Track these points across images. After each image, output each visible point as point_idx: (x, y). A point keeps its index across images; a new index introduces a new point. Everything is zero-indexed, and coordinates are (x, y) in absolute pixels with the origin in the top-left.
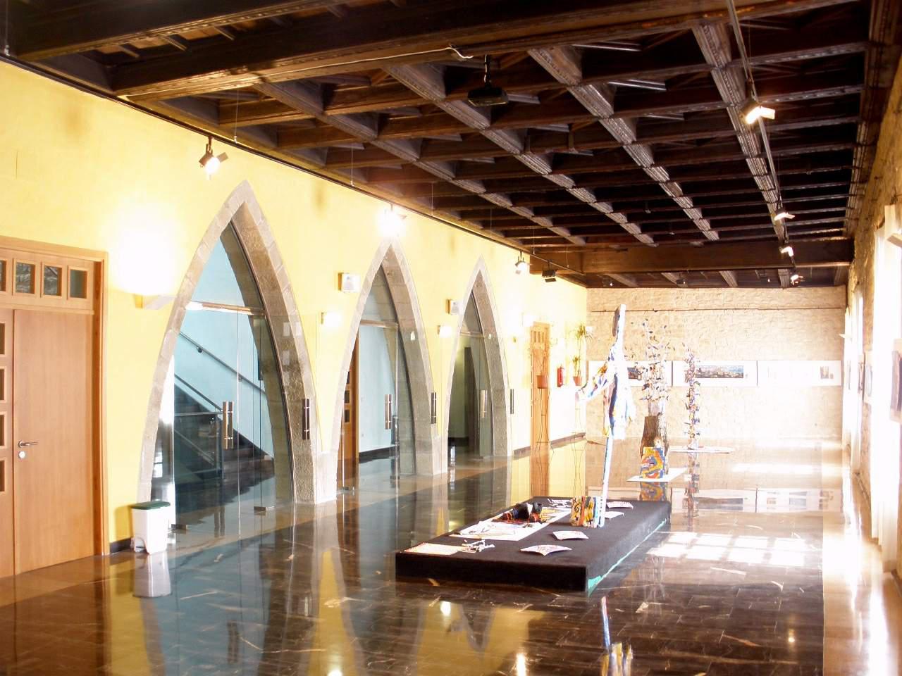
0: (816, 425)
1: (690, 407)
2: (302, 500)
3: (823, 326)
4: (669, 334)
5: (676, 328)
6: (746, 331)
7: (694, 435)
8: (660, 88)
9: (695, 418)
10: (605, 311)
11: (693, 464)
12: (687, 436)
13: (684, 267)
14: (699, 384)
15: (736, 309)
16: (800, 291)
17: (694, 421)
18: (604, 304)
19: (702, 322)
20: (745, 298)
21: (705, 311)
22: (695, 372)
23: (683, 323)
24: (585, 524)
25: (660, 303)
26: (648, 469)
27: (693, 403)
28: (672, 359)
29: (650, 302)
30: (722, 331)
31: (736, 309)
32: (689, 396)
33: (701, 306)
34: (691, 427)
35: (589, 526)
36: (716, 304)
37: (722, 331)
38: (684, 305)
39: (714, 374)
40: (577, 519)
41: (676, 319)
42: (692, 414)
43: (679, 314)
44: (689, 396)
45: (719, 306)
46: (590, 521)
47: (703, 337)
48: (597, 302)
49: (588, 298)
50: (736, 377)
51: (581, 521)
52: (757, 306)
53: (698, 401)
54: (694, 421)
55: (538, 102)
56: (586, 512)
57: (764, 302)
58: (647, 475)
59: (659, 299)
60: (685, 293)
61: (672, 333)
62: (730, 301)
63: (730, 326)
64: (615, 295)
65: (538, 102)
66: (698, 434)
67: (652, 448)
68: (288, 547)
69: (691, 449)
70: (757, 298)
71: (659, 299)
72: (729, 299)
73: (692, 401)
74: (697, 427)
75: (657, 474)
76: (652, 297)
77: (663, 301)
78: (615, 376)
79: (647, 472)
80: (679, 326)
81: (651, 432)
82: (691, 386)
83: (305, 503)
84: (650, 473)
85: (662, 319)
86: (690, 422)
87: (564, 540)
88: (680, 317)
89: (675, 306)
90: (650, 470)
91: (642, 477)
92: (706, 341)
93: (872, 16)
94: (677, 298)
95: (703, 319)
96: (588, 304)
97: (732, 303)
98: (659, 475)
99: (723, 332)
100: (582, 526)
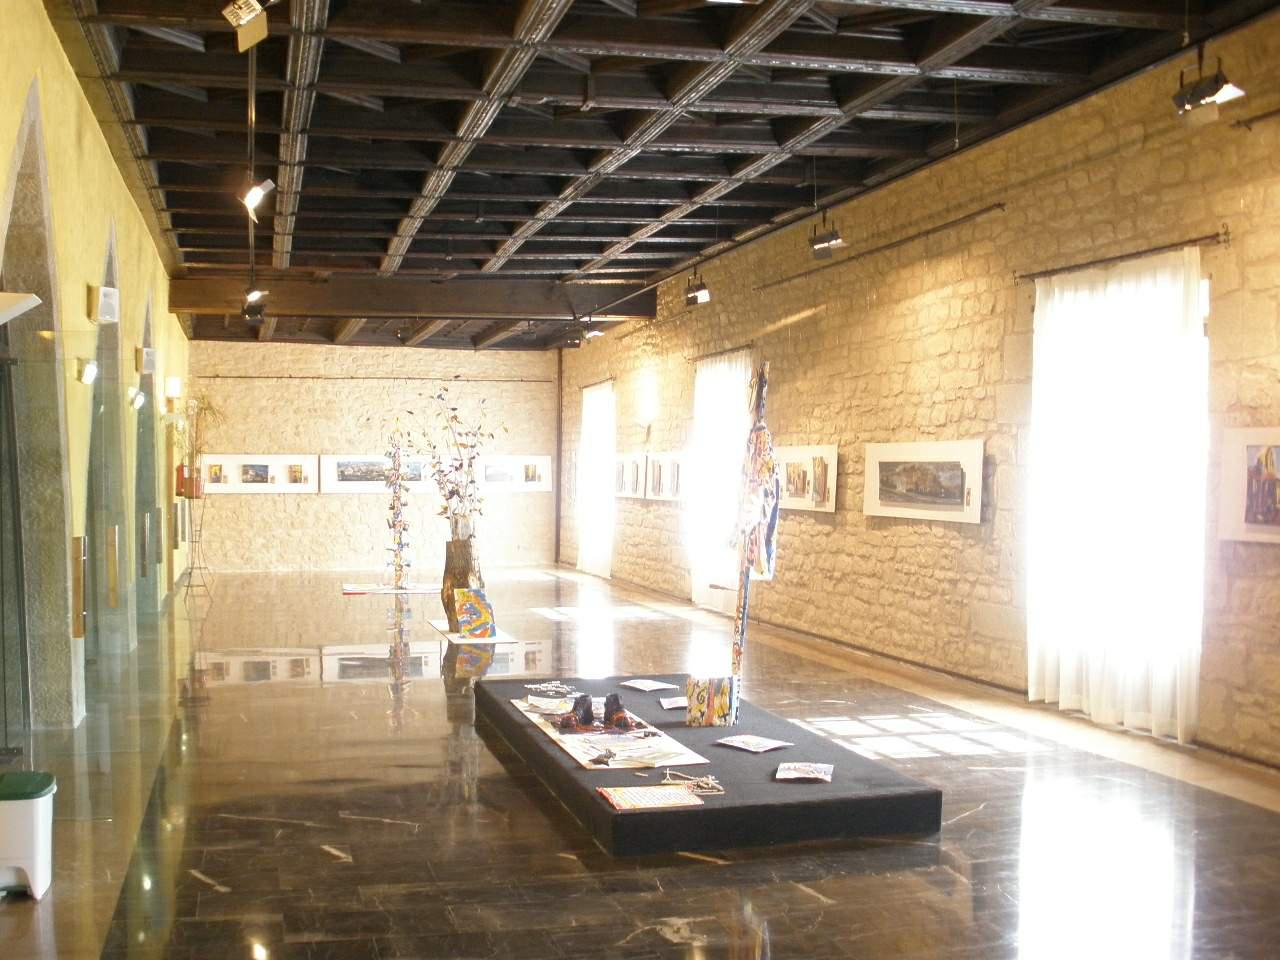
0: (519, 547)
1: (394, 525)
2: (46, 723)
3: (528, 406)
4: (314, 414)
5: (323, 404)
6: (424, 412)
8: (392, 55)
10: (218, 376)
11: (401, 610)
12: (392, 569)
13: (413, 311)
14: (407, 490)
15: (409, 378)
16: (497, 356)
17: (401, 545)
18: (215, 365)
19: (361, 396)
20: (422, 362)
23: (334, 398)
24: (717, 721)
25: (301, 366)
26: (469, 623)
27: (399, 519)
28: (318, 449)
29: (285, 365)
30: (391, 411)
32: (392, 508)
33: (361, 373)
34: (396, 555)
35: (723, 723)
36: (382, 371)
38: (336, 371)
39: (380, 475)
40: (703, 714)
41: (324, 391)
43: (329, 385)
44: (392, 508)
45: (387, 373)
46: (725, 716)
48: (203, 363)
49: (190, 356)
50: (258, 494)
51: (710, 717)
52: (439, 376)
53: (406, 515)
55: (201, 49)
56: (717, 702)
57: (449, 369)
58: (472, 632)
59: (299, 360)
60: (338, 352)
61: (319, 413)
62: (400, 367)
64: (231, 352)
65: (201, 49)
66: (408, 565)
67: (466, 590)
69: (401, 588)
70: (440, 363)
71: (299, 360)
72: (400, 363)
73: (397, 515)
74: (406, 553)
75: (486, 630)
76: (289, 357)
77: (306, 363)
79: (469, 627)
80: (329, 402)
81: (459, 567)
83: (51, 728)
84: (475, 629)
85: (303, 391)
86: (396, 547)
87: (766, 751)
88: (330, 389)
89: (322, 372)
90: (474, 625)
91: (464, 637)
93: (291, 54)
94: (326, 359)
96: (190, 365)
97: (405, 369)
99: (392, 413)
100: (711, 725)
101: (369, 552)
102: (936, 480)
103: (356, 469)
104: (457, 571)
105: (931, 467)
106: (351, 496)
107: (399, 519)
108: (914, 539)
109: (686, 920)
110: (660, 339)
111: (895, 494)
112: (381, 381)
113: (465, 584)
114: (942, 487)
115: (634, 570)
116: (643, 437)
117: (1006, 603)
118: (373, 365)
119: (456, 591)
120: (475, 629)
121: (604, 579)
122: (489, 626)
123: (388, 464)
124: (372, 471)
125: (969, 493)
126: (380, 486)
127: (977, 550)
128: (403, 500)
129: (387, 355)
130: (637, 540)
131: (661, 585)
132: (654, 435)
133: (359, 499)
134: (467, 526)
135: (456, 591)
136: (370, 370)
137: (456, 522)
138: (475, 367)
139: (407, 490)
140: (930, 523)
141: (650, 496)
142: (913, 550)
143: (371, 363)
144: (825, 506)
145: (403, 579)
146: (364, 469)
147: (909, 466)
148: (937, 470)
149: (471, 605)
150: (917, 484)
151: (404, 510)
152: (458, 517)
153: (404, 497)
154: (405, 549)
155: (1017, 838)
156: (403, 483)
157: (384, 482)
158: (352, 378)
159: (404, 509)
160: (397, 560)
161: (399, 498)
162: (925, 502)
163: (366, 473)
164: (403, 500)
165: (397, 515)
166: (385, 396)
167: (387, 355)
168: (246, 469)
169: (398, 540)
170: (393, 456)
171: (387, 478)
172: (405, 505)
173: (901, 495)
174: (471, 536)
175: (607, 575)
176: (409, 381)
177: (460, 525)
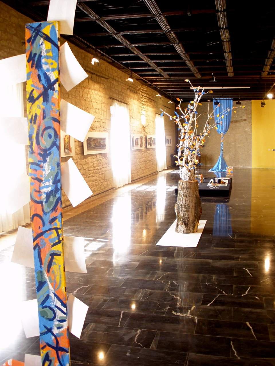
102: (100, 143)
105: (99, 139)
108: (93, 160)
109: (270, 341)
111: (91, 147)
114: (101, 144)
117: (110, 170)
127: (104, 159)
140: (96, 155)
142: (93, 163)
144: (70, 154)
147: (94, 139)
148: (100, 140)
150: (96, 144)
155: (166, 212)
162: (98, 149)
168: (142, 137)
173: (93, 147)
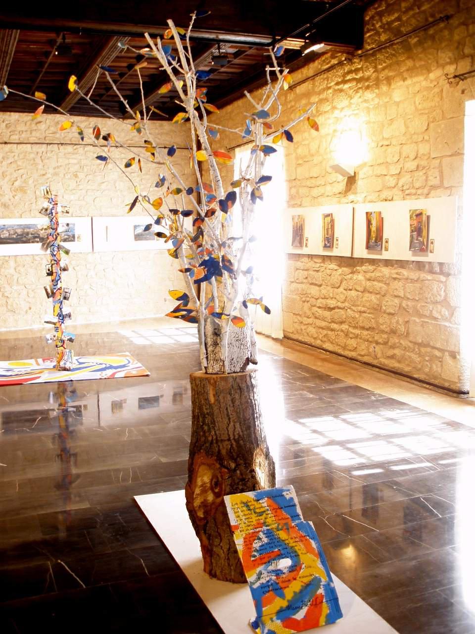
1: (53, 294)
6: (76, 176)
7: (63, 342)
9: (64, 313)
14: (67, 252)
15: (62, 144)
17: (62, 317)
21: (20, 146)
22: (60, 230)
27: (59, 286)
30: (44, 175)
31: (62, 144)
32: (50, 273)
33: (15, 138)
34: (57, 329)
37: (44, 175)
42: (58, 305)
44: (50, 273)
47: (17, 184)
54: (62, 317)
63: (55, 168)
67: (250, 495)
68: (101, 95)
72: (52, 129)
73: (55, 282)
75: (317, 603)
78: (131, 208)
82: (53, 255)
84: (293, 607)
86: (56, 320)
90: (289, 593)
92: (22, 190)
95: (16, 158)
98: (326, 609)
99: (46, 177)
101: (26, 312)
103: (12, 232)
104: (224, 448)
106: (7, 258)
107: (59, 286)
110: (372, 70)
112: (36, 147)
113: (247, 483)
115: (326, 336)
116: (342, 186)
118: (26, 131)
119: (228, 499)
120: (293, 607)
121: (276, 340)
122: (321, 591)
123: (43, 222)
124: (28, 234)
125: (387, 242)
126: (35, 248)
128: (62, 264)
129: (40, 122)
130: (332, 303)
131: (383, 360)
132: (360, 183)
133: (16, 262)
134: (239, 340)
135: (228, 499)
136: (23, 136)
137: (217, 333)
138: (123, 134)
139: (67, 252)
141: (361, 252)
143: (24, 129)
145: (66, 357)
146: (19, 231)
149: (269, 534)
151: (64, 275)
152: (223, 322)
153: (64, 261)
154: (67, 322)
156: (62, 244)
157: (40, 244)
158: (6, 143)
159: (64, 275)
160: (58, 334)
161: (57, 262)
163: (22, 235)
164: (62, 264)
165: (55, 282)
166: (38, 160)
167: (40, 122)
169: (57, 311)
170: (48, 212)
171: (42, 240)
172: (65, 270)
174: (248, 361)
175: (281, 336)
176: (61, 147)
177: (226, 339)
